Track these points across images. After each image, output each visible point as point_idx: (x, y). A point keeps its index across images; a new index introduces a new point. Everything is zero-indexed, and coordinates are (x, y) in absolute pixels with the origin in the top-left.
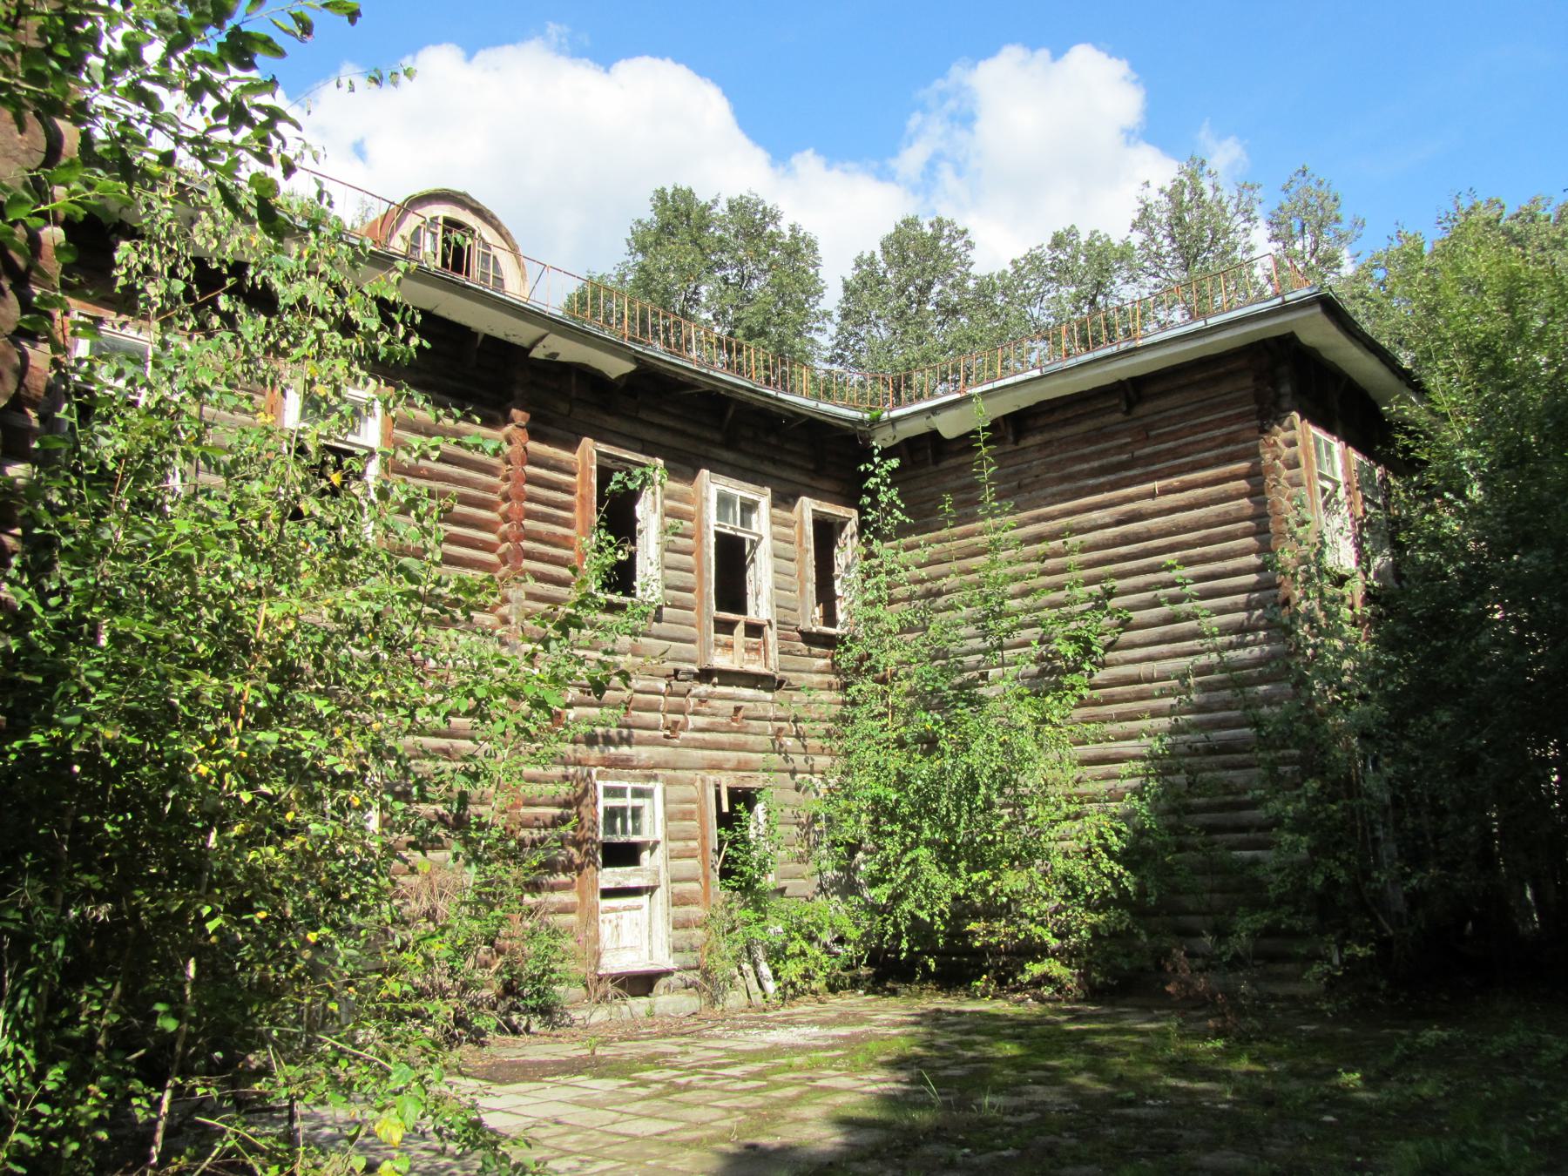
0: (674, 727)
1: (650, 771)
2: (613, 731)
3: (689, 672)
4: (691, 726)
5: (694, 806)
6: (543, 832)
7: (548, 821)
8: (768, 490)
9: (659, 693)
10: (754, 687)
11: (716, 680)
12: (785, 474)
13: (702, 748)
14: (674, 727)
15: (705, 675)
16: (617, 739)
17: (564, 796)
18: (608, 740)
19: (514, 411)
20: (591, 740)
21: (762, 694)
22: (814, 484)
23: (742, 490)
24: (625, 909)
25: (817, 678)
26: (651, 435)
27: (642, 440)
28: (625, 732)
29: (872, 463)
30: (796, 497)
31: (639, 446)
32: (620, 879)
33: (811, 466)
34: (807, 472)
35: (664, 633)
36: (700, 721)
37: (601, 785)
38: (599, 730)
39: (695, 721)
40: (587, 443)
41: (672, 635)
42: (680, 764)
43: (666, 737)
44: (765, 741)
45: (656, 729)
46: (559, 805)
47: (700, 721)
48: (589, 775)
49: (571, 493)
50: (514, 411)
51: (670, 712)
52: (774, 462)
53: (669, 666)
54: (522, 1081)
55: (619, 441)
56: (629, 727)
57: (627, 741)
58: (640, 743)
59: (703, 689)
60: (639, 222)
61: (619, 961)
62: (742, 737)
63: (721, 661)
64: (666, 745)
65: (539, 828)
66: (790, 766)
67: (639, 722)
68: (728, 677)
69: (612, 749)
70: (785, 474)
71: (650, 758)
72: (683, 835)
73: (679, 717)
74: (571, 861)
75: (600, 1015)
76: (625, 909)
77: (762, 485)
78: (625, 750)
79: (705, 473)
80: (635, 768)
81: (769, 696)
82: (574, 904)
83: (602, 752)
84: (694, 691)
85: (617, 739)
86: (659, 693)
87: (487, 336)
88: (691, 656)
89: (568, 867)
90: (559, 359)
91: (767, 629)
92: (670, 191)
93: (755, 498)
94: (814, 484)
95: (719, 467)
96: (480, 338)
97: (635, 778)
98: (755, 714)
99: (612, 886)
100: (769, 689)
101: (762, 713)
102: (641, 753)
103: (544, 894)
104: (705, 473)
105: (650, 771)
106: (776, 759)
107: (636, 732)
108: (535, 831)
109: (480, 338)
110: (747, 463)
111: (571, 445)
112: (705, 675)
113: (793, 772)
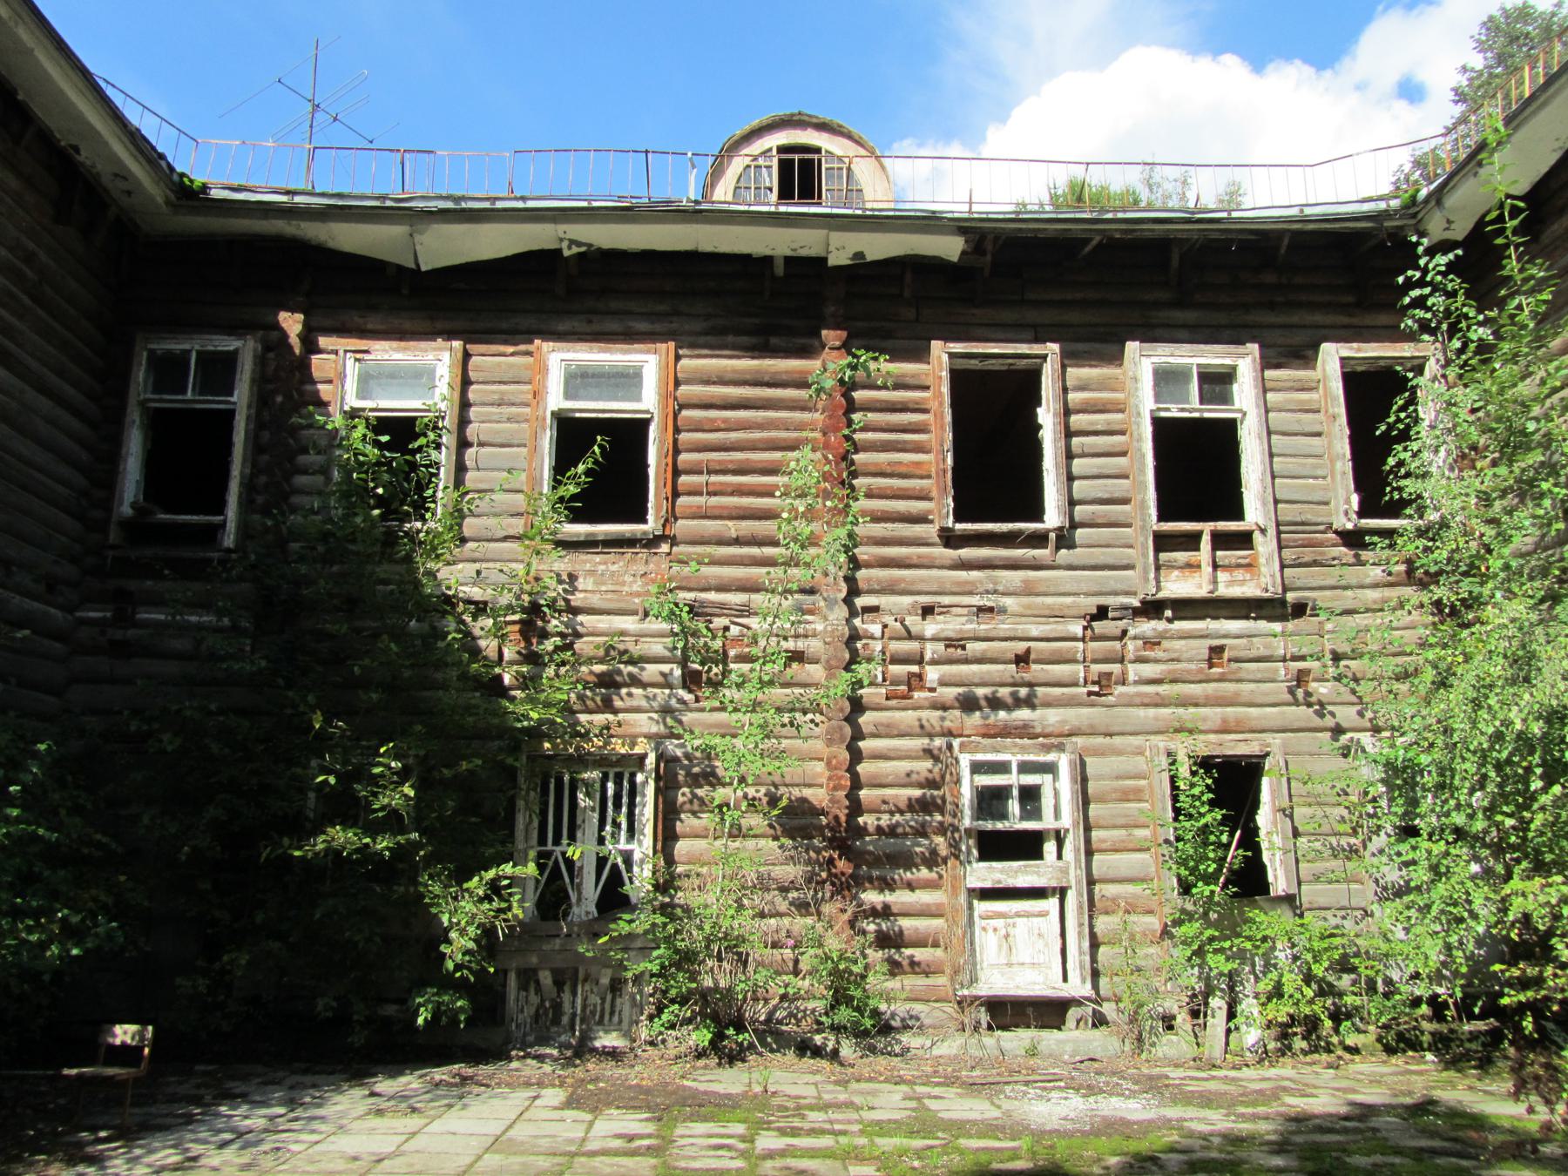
0: (1104, 681)
1: (1057, 739)
2: (1004, 692)
3: (1125, 608)
4: (1131, 677)
5: (1143, 782)
6: (897, 817)
7: (903, 805)
8: (1254, 348)
9: (1075, 639)
10: (1247, 618)
11: (1168, 613)
12: (1295, 319)
13: (1157, 705)
14: (1104, 681)
15: (1152, 608)
16: (1009, 700)
17: (925, 774)
18: (995, 703)
19: (824, 332)
20: (968, 704)
21: (1263, 625)
22: (1355, 321)
23: (1213, 356)
24: (1018, 915)
25: (1372, 595)
26: (1032, 316)
27: (1034, 326)
28: (1023, 692)
29: (1417, 268)
30: (1315, 347)
31: (1030, 334)
32: (998, 876)
33: (1350, 299)
34: (1343, 308)
35: (1076, 562)
36: (1149, 670)
37: (965, 760)
38: (981, 692)
39: (1133, 671)
40: (936, 346)
41: (1092, 562)
42: (1115, 729)
43: (1090, 694)
44: (1280, 690)
45: (1076, 684)
46: (920, 786)
47: (1149, 670)
48: (950, 747)
49: (925, 411)
50: (824, 332)
51: (1095, 661)
52: (1272, 306)
53: (1090, 604)
54: (1054, 1124)
55: (1010, 335)
56: (1031, 685)
57: (1029, 703)
58: (1048, 704)
59: (1148, 627)
60: (1464, 69)
61: (996, 981)
62: (1230, 687)
63: (1178, 586)
64: (1093, 705)
65: (892, 813)
66: (1329, 722)
67: (1042, 678)
68: (1186, 608)
69: (1002, 714)
70: (1295, 319)
71: (1064, 722)
72: (1122, 821)
73: (1115, 668)
74: (934, 852)
75: (950, 1046)
76: (1018, 915)
77: (1240, 342)
78: (1024, 714)
79: (1132, 347)
80: (1036, 736)
81: (1277, 627)
82: (939, 905)
83: (986, 718)
84: (1132, 632)
85: (1009, 700)
86: (1075, 639)
87: (789, 260)
88: (1140, 584)
89: (932, 860)
90: (869, 258)
91: (1257, 536)
92: (1497, 13)
93: (1228, 361)
94: (1355, 321)
95: (1151, 334)
96: (779, 270)
97: (1023, 749)
98: (1254, 653)
99: (988, 884)
100: (1283, 618)
101: (1263, 652)
102: (1050, 718)
103: (898, 892)
104: (1132, 347)
105: (1057, 739)
106: (1303, 714)
107: (1040, 690)
108: (886, 817)
109: (779, 270)
110: (1222, 318)
111: (921, 355)
112: (1152, 608)
113: (1338, 731)
